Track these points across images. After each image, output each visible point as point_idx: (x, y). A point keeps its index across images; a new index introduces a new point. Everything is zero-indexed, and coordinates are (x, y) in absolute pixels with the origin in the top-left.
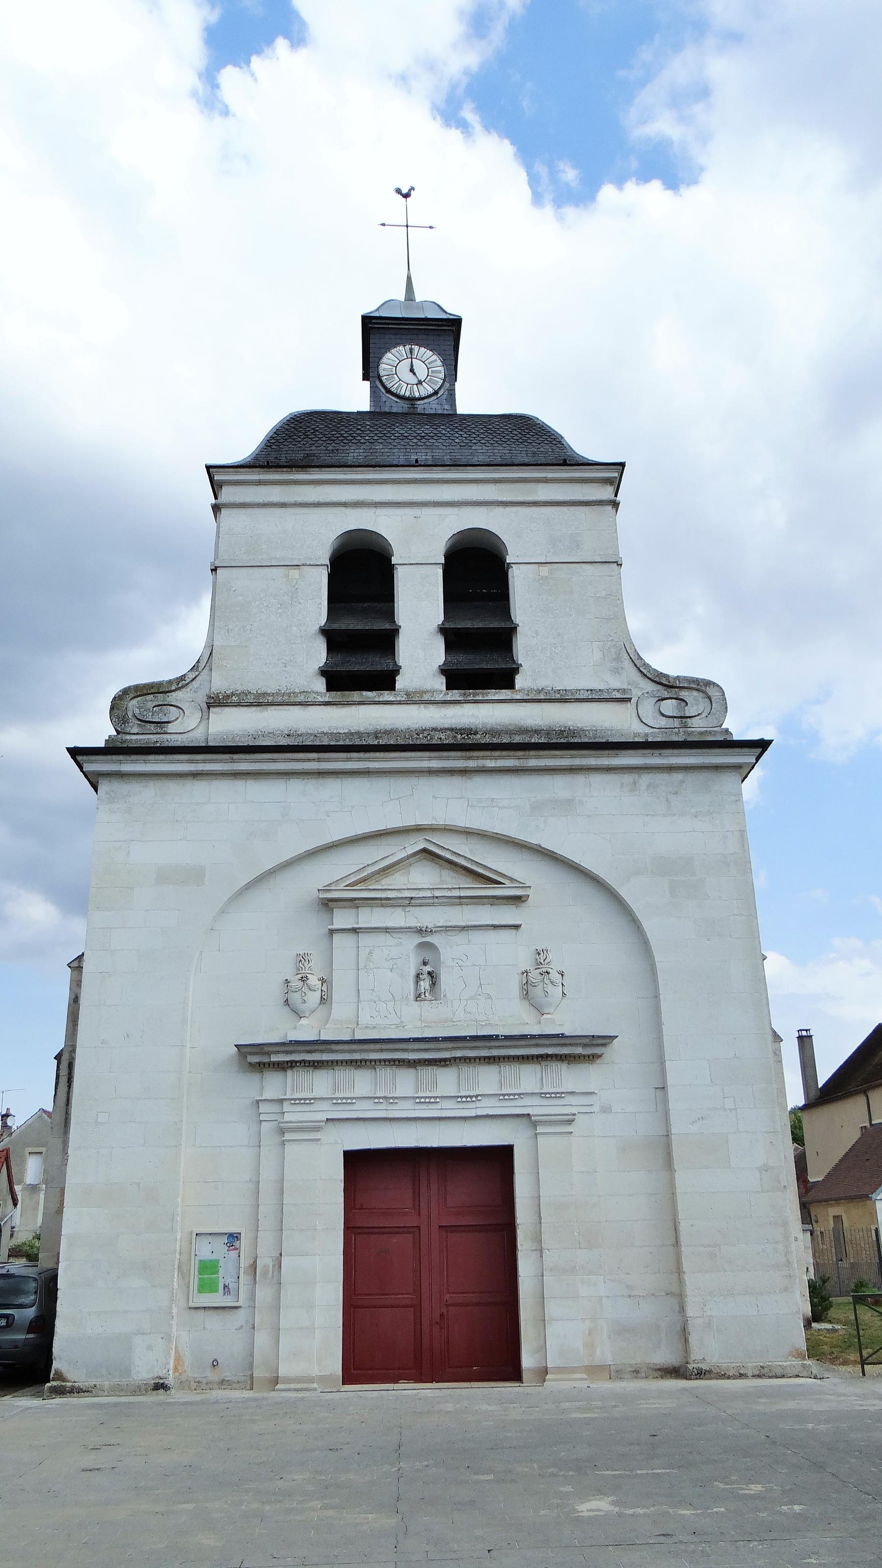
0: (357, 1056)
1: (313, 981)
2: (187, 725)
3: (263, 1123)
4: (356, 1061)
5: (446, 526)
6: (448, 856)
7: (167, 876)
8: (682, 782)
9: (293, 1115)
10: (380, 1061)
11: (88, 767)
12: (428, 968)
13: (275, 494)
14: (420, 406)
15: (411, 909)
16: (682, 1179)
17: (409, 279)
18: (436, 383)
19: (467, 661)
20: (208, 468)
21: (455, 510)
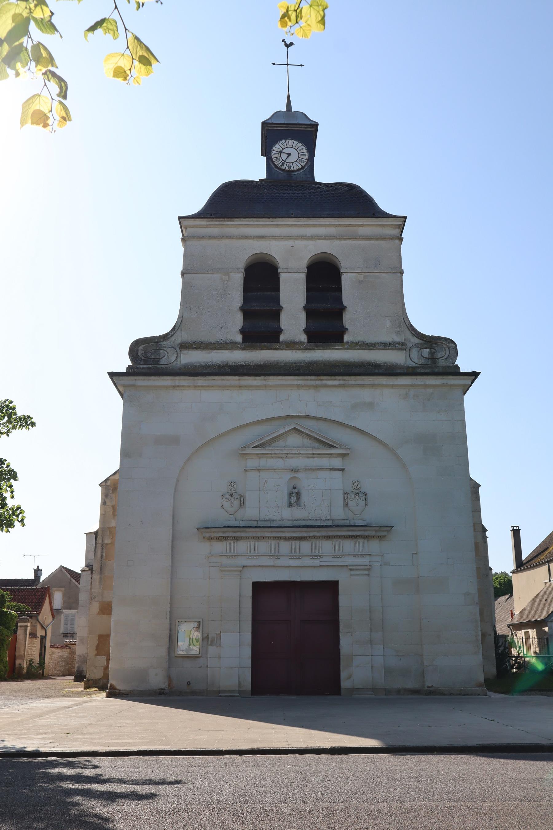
5: (308, 251)
6: (307, 432)
15: (287, 459)
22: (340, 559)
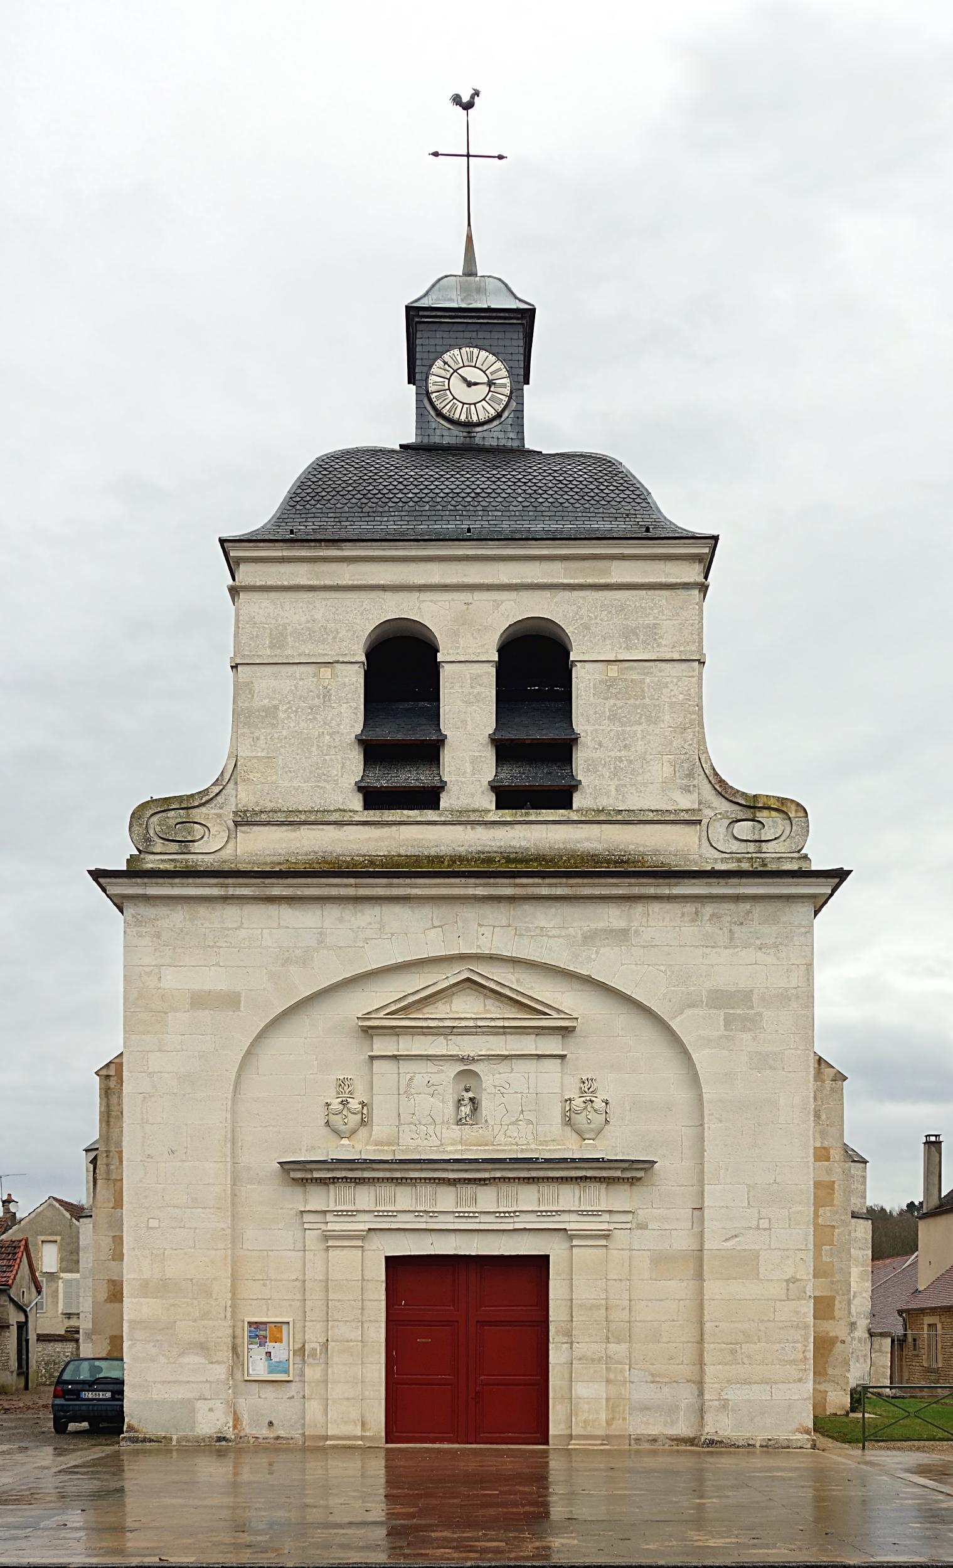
0: (398, 1175)
1: (354, 1104)
2: (213, 844)
3: (239, 668)
4: (397, 1179)
6: (493, 986)
7: (199, 1001)
8: (748, 912)
9: (336, 1225)
10: (420, 1179)
11: (112, 890)
12: (470, 1094)
13: (301, 574)
14: (481, 436)
16: (712, 1288)
17: (469, 239)
18: (499, 401)
19: (520, 776)
20: (222, 541)
21: (513, 595)
22: (557, 1219)
